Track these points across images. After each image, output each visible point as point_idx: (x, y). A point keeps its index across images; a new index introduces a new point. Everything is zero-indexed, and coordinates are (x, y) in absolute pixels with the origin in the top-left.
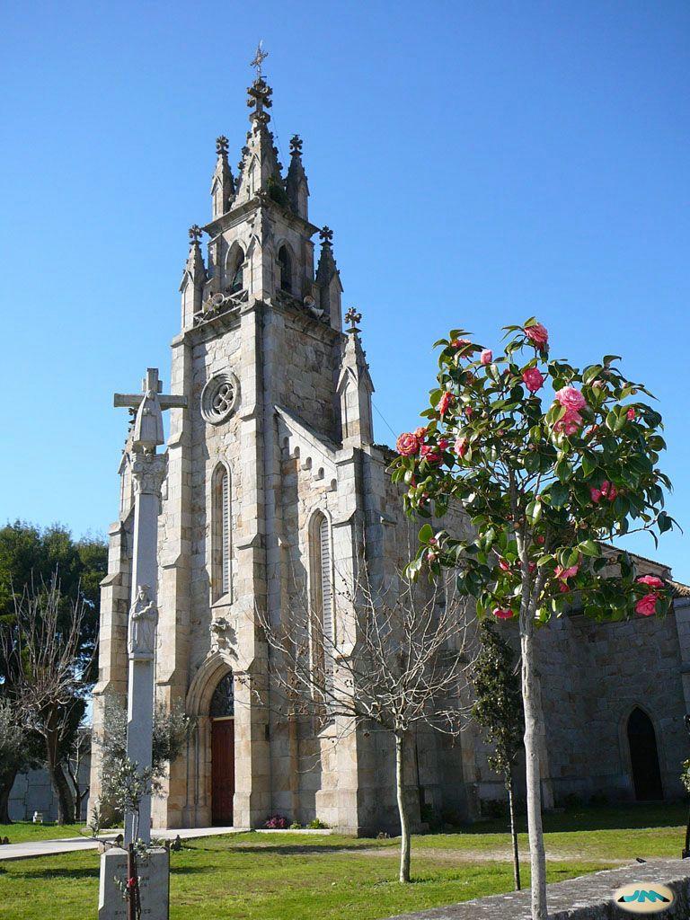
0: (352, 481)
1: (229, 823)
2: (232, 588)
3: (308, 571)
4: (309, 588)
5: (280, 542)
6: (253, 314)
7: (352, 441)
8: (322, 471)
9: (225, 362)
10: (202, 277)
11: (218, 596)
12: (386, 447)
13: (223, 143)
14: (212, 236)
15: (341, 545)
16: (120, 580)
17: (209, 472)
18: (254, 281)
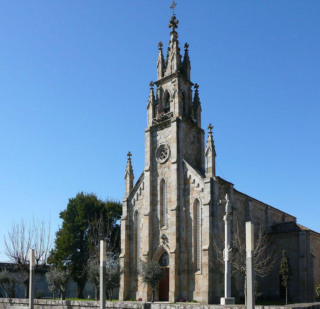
0: (209, 189)
1: (168, 301)
2: (167, 224)
3: (193, 219)
4: (193, 225)
5: (184, 209)
6: (176, 122)
7: (209, 175)
8: (198, 184)
9: (164, 140)
10: (155, 103)
11: (162, 226)
12: (219, 177)
13: (161, 45)
14: (158, 86)
15: (205, 213)
16: (127, 218)
17: (159, 181)
18: (175, 108)
